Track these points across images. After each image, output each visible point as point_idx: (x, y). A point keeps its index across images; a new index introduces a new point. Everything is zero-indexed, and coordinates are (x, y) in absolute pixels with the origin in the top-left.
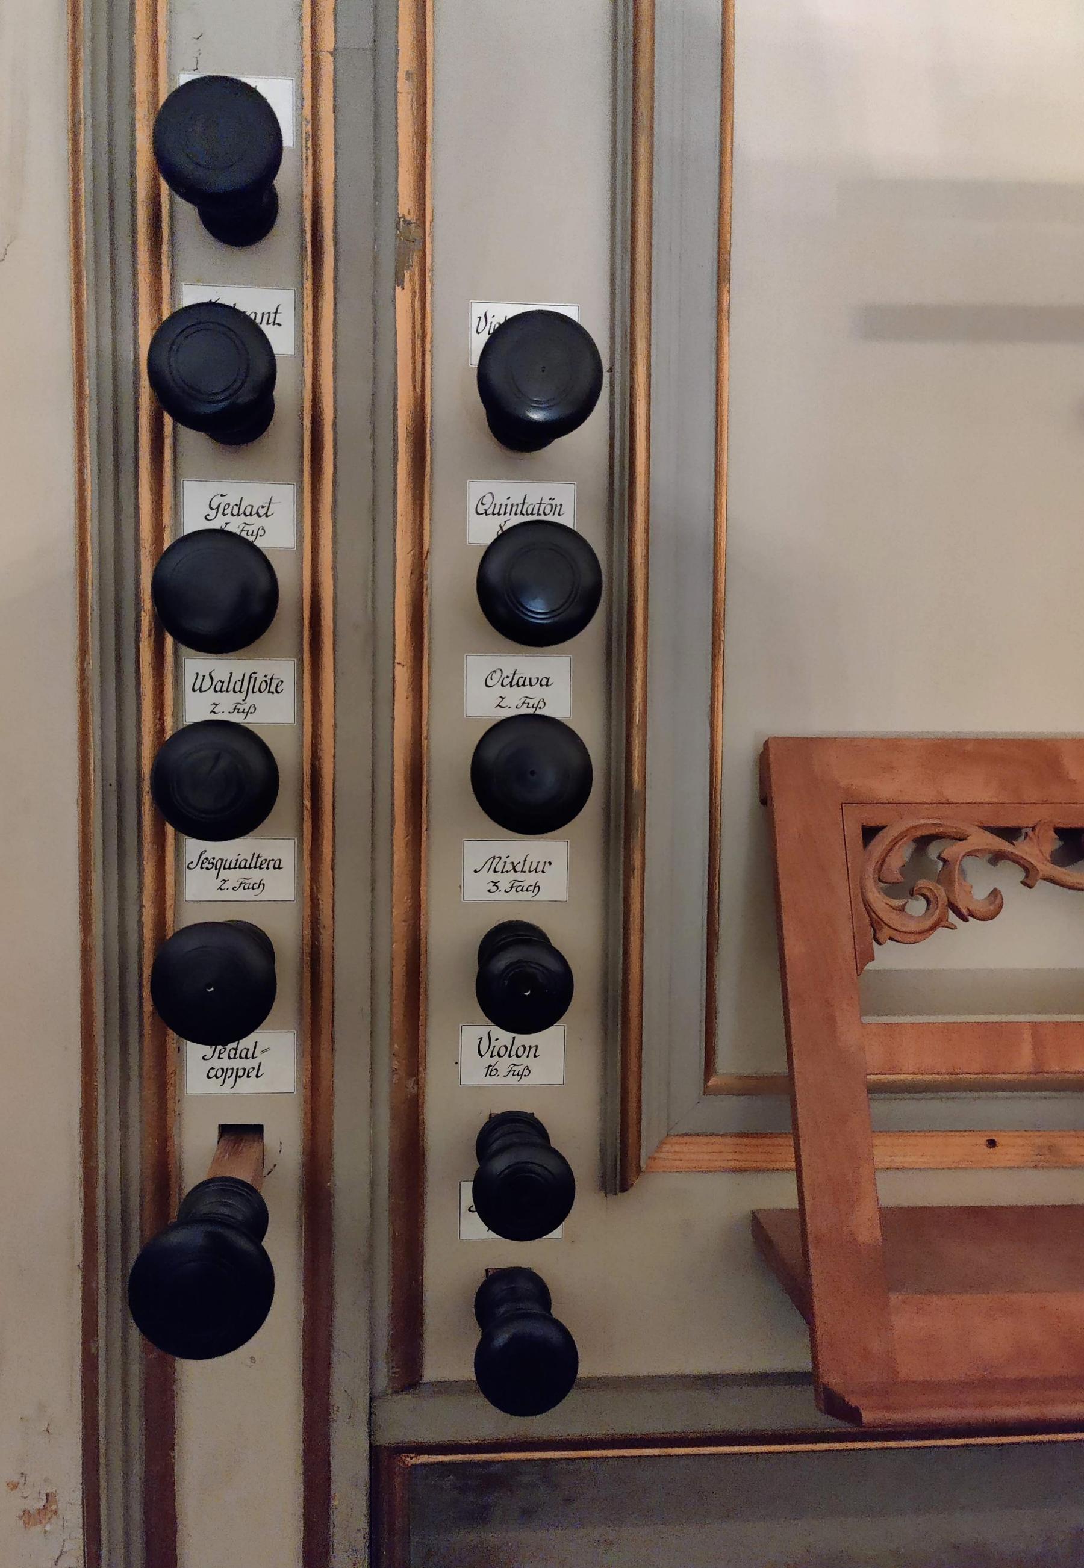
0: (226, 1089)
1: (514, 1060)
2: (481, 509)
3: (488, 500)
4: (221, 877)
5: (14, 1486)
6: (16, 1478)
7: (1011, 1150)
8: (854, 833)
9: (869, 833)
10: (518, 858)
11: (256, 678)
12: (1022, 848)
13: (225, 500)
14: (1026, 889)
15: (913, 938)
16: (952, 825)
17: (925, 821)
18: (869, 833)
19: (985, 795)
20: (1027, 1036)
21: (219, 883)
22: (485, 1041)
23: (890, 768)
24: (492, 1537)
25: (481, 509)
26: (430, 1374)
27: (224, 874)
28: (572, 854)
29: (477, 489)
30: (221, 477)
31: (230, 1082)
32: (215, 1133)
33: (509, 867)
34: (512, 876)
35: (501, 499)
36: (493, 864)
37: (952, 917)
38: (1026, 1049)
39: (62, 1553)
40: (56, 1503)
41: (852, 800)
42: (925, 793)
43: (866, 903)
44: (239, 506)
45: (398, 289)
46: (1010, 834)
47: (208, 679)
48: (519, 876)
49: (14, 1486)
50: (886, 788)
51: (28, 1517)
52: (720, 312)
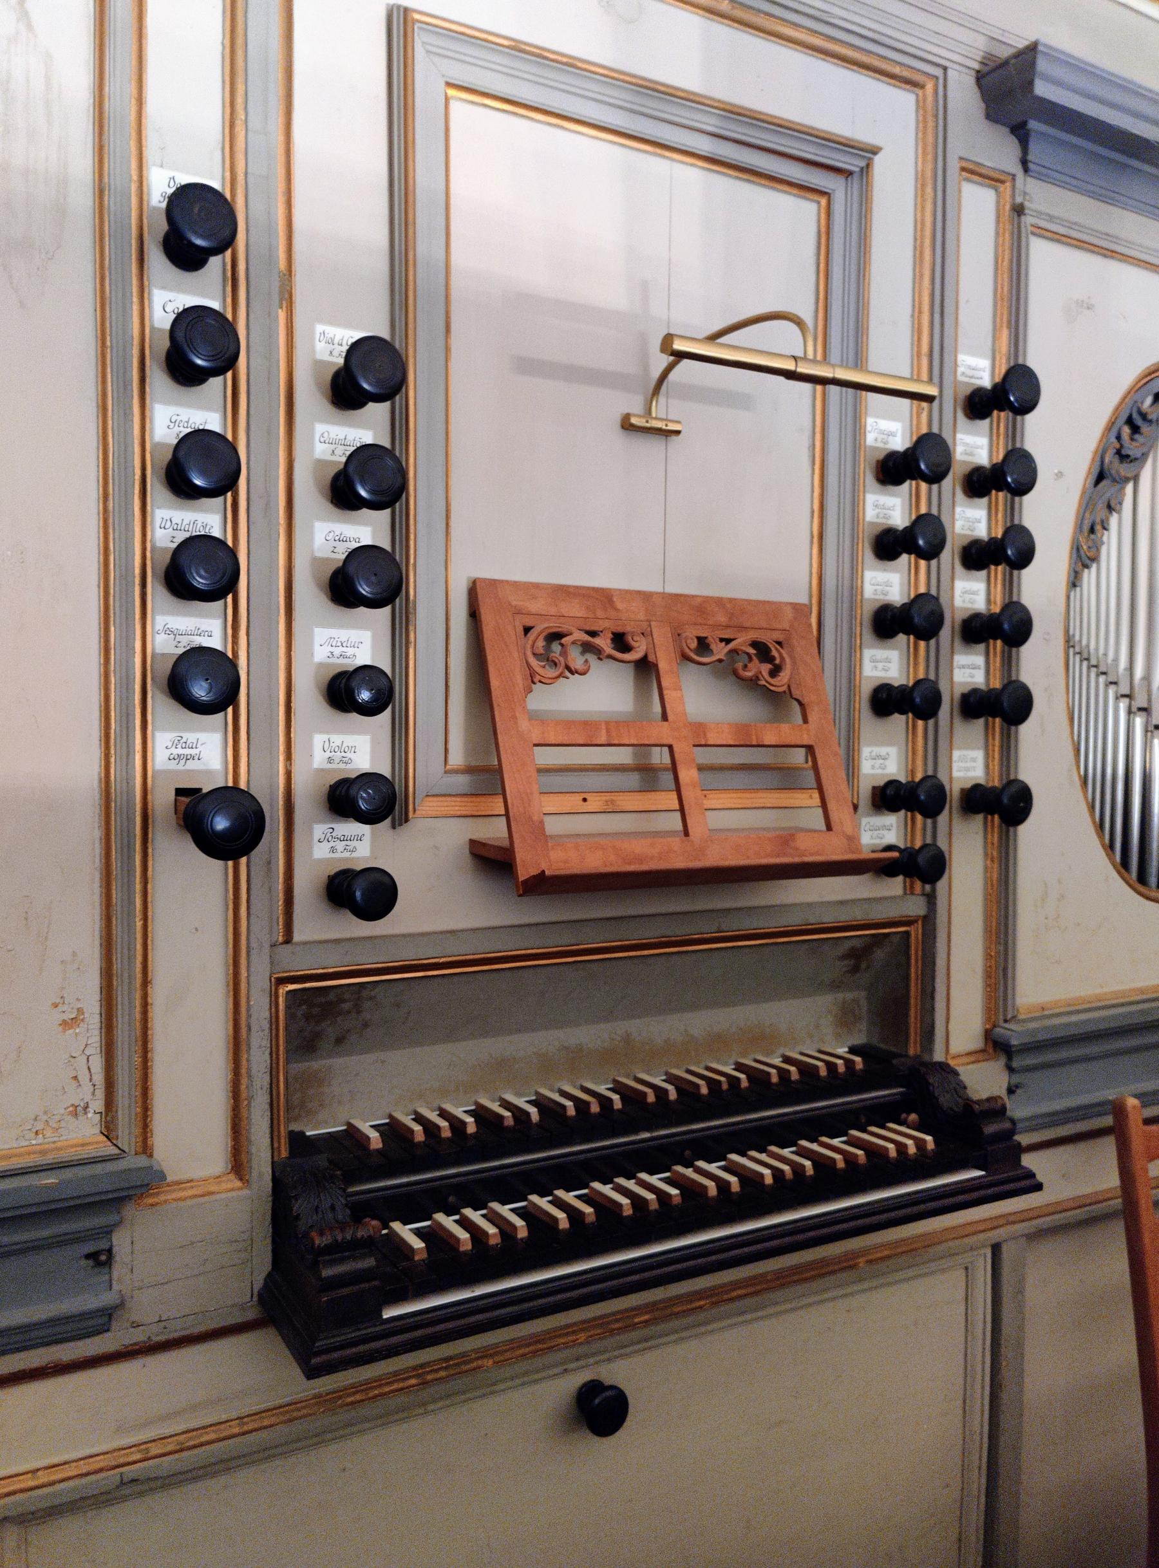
0: (180, 767)
1: (343, 754)
2: (322, 440)
3: (326, 435)
4: (177, 640)
5: (56, 1006)
6: (58, 1000)
7: (595, 803)
8: (520, 630)
9: (527, 630)
10: (343, 639)
11: (1032, 225)
12: (597, 641)
13: (179, 418)
14: (653, 448)
15: (550, 681)
16: (565, 628)
17: (554, 625)
18: (527, 630)
19: (581, 613)
20: (603, 727)
21: (175, 643)
22: (327, 743)
23: (534, 598)
24: (315, 1065)
25: (322, 440)
26: (297, 937)
27: (179, 638)
28: (374, 637)
29: (320, 428)
30: (178, 403)
31: (182, 762)
32: (173, 793)
33: (339, 644)
34: (341, 649)
35: (333, 435)
36: (330, 641)
37: (567, 674)
38: (604, 732)
39: (86, 1045)
40: (83, 1014)
41: (518, 612)
42: (553, 611)
43: (527, 663)
44: (188, 422)
45: (280, 311)
46: (593, 634)
47: (169, 522)
48: (345, 649)
49: (56, 1006)
50: (535, 607)
51: (65, 1024)
52: (447, 349)
